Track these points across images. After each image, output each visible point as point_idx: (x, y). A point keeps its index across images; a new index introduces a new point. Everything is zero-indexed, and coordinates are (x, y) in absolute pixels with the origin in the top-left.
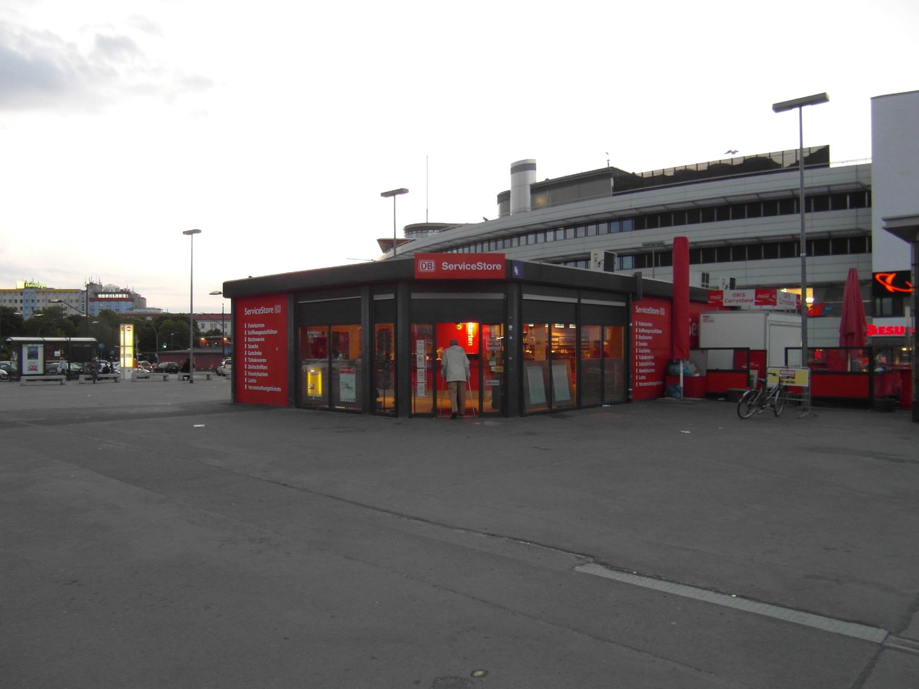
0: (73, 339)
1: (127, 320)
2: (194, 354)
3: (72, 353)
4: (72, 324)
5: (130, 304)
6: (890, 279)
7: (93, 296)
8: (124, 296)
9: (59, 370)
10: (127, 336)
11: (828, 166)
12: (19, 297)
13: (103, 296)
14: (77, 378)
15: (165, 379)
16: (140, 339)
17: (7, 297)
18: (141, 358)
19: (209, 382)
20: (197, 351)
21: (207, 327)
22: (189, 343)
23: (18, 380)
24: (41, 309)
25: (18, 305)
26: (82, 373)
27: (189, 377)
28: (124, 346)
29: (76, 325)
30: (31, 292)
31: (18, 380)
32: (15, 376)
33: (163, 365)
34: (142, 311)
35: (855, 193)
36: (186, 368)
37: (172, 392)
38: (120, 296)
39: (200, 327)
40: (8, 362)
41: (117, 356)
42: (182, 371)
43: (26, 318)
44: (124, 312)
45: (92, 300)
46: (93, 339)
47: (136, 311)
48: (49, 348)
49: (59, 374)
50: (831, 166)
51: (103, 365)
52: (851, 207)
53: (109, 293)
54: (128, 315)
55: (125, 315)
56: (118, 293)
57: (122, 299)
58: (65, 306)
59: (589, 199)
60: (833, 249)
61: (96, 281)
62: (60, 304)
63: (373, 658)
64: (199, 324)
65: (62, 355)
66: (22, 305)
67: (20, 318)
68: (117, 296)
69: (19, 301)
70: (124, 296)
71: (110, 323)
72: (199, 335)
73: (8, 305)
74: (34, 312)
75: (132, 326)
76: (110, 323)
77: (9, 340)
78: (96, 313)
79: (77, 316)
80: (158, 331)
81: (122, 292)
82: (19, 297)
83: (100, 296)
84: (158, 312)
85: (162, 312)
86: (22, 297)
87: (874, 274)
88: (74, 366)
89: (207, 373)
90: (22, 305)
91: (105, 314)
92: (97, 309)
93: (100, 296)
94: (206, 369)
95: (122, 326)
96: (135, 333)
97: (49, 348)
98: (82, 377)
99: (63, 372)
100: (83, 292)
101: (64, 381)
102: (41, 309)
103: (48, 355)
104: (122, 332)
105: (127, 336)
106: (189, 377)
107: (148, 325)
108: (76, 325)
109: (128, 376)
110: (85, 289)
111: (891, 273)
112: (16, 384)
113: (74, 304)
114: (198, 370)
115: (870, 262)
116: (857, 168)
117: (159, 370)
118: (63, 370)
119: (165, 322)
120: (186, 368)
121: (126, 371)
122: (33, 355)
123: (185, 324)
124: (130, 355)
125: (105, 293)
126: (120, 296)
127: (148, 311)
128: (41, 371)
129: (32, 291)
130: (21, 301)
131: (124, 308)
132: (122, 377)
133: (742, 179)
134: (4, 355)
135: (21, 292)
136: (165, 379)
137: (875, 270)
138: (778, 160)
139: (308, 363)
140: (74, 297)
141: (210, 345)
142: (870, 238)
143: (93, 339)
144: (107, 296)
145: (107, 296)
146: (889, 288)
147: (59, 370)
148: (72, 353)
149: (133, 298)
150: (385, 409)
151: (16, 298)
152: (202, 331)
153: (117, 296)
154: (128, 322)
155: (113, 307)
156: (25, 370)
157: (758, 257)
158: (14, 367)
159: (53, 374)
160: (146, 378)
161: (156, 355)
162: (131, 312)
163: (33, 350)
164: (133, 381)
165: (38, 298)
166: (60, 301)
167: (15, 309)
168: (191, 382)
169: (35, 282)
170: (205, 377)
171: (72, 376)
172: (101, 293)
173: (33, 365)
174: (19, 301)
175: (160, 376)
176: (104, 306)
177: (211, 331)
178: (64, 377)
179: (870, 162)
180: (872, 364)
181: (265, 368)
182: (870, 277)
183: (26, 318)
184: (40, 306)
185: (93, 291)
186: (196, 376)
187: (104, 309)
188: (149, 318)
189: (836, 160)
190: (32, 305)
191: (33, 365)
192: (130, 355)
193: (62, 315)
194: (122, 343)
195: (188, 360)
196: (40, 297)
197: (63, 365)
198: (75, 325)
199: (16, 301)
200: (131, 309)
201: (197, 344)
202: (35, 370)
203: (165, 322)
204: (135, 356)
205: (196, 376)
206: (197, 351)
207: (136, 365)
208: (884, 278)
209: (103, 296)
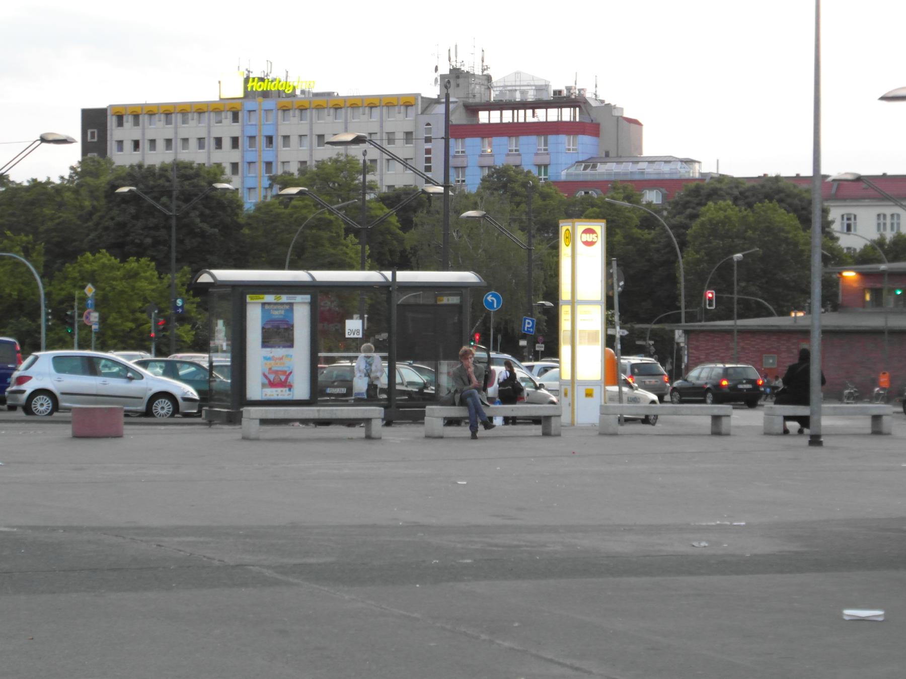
0: (404, 276)
1: (580, 203)
2: (828, 334)
3: (407, 326)
4: (394, 220)
5: (585, 144)
7: (459, 118)
8: (567, 114)
9: (360, 385)
10: (584, 265)
12: (227, 129)
13: (495, 117)
14: (418, 418)
15: (717, 428)
16: (629, 279)
17: (193, 129)
18: (629, 348)
19: (877, 443)
20: (834, 320)
21: (861, 227)
22: (807, 292)
23: (234, 419)
24: (294, 169)
25: (226, 156)
26: (434, 399)
27: (804, 421)
28: (573, 303)
29: (407, 224)
30: (265, 104)
31: (234, 419)
32: (222, 403)
33: (701, 374)
34: (629, 167)
36: (795, 388)
37: (741, 478)
38: (552, 115)
39: (836, 227)
40: (203, 359)
41: (548, 344)
42: (782, 398)
43: (250, 202)
44: (563, 176)
45: (453, 132)
46: (468, 277)
47: (606, 170)
48: (330, 306)
49: (359, 402)
51: (500, 371)
53: (514, 106)
54: (585, 184)
55: (570, 186)
56: (546, 105)
57: (557, 128)
58: (373, 153)
61: (470, 64)
62: (356, 151)
64: (836, 214)
65: (368, 334)
66: (235, 156)
67: (228, 204)
68: (541, 115)
69: (227, 143)
70: (567, 114)
71: (532, 212)
72: (835, 258)
73: (194, 156)
74: (273, 179)
75: (599, 228)
76: (532, 212)
77: (205, 278)
78: (472, 182)
79: (408, 191)
80: (683, 244)
81: (560, 100)
82: (227, 129)
83: (483, 117)
84: (683, 172)
85: (695, 172)
86: (235, 130)
88: (409, 375)
89: (878, 407)
90: (235, 156)
91: (502, 181)
92: (477, 159)
93: (483, 117)
94: (863, 394)
95: (565, 227)
96: (611, 251)
97: (330, 306)
98: (435, 414)
99: (371, 396)
100: (429, 103)
101: (377, 426)
102: (294, 169)
103: (326, 336)
104: (565, 251)
105: (584, 265)
106: (804, 421)
107: (648, 222)
108: (407, 224)
109: (588, 413)
110: (433, 91)
112: (225, 433)
113: (401, 149)
114: (834, 394)
117: (693, 395)
118: (372, 387)
119: (711, 211)
120: (795, 388)
121: (580, 392)
122: (278, 334)
123: (783, 218)
124: (592, 337)
125: (500, 106)
126: (552, 115)
127: (651, 171)
128: (301, 389)
129: (269, 104)
130: (235, 142)
131: (565, 160)
132: (565, 419)
134: (185, 332)
135: (233, 110)
136: (717, 428)
139: (855, 285)
140: (398, 123)
141: (877, 294)
143: (468, 277)
144: (508, 116)
145: (508, 116)
147: (360, 385)
148: (407, 326)
149: (591, 120)
151: (218, 131)
152: (846, 242)
153: (541, 115)
154: (581, 210)
155: (526, 154)
156: (255, 389)
158: (223, 380)
159: (340, 400)
160: (646, 420)
161: (679, 336)
162: (589, 175)
163: (278, 313)
164: (605, 433)
165: (284, 129)
166: (358, 140)
167: (216, 172)
168: (815, 441)
169: (277, 73)
170: (865, 424)
171: (403, 408)
172: (490, 107)
173: (278, 367)
174: (227, 143)
175: (699, 416)
176: (498, 151)
177: (881, 243)
178: (376, 412)
180: (746, 231)
183: (250, 202)
184: (291, 158)
185: (463, 103)
186: (831, 418)
187: (500, 162)
188: (652, 197)
190: (268, 156)
191: (278, 367)
192: (592, 337)
193: (368, 187)
194: (565, 293)
195: (805, 356)
196: (292, 126)
197: (364, 368)
198: (400, 226)
199: (219, 142)
200: (590, 163)
201: (832, 298)
202: (285, 384)
203: (711, 211)
204: (610, 341)
205: (831, 418)
206: (834, 320)
207: (612, 373)
209: (495, 117)
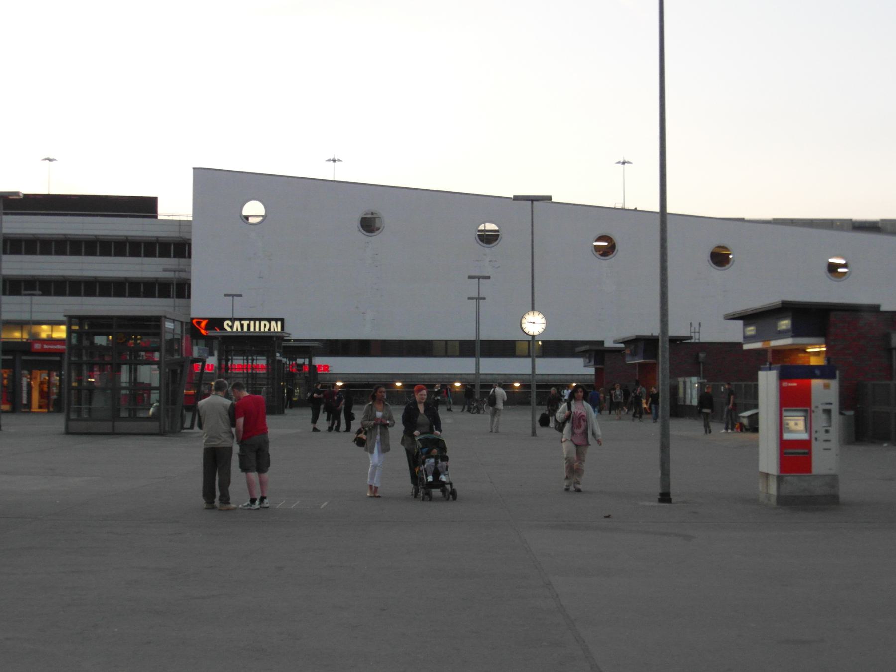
6: (203, 324)
11: (156, 217)
35: (177, 246)
50: (160, 217)
52: (160, 257)
59: (12, 214)
60: (177, 292)
63: (608, 517)
87: (192, 319)
111: (204, 319)
115: (189, 306)
116: (180, 223)
133: (81, 218)
137: (192, 316)
138: (880, 225)
142: (189, 285)
146: (203, 331)
150: (53, 403)
157: (62, 294)
179: (190, 218)
181: (257, 330)
182: (189, 320)
189: (164, 211)
208: (199, 323)
